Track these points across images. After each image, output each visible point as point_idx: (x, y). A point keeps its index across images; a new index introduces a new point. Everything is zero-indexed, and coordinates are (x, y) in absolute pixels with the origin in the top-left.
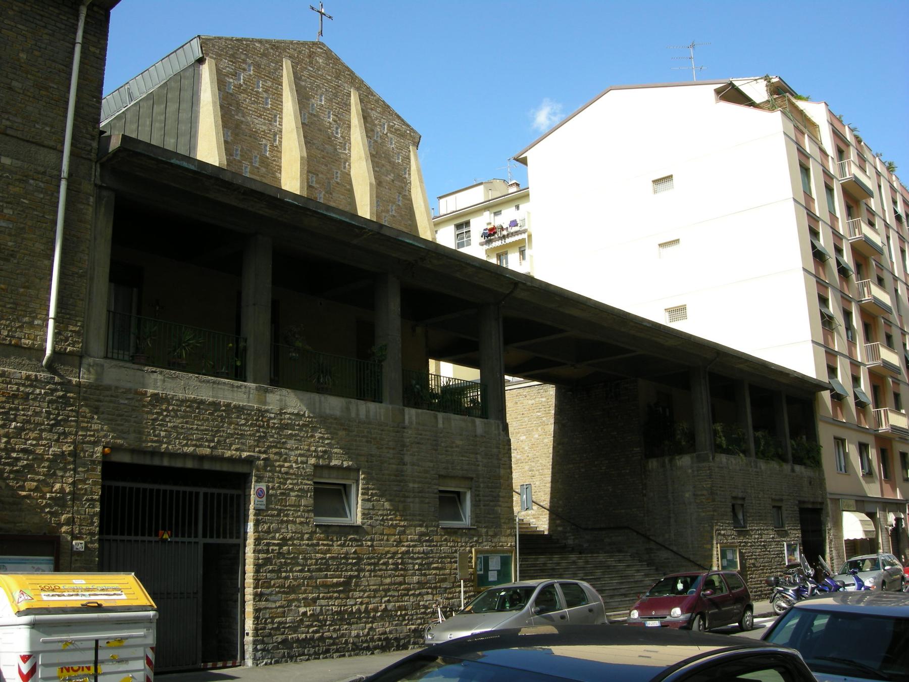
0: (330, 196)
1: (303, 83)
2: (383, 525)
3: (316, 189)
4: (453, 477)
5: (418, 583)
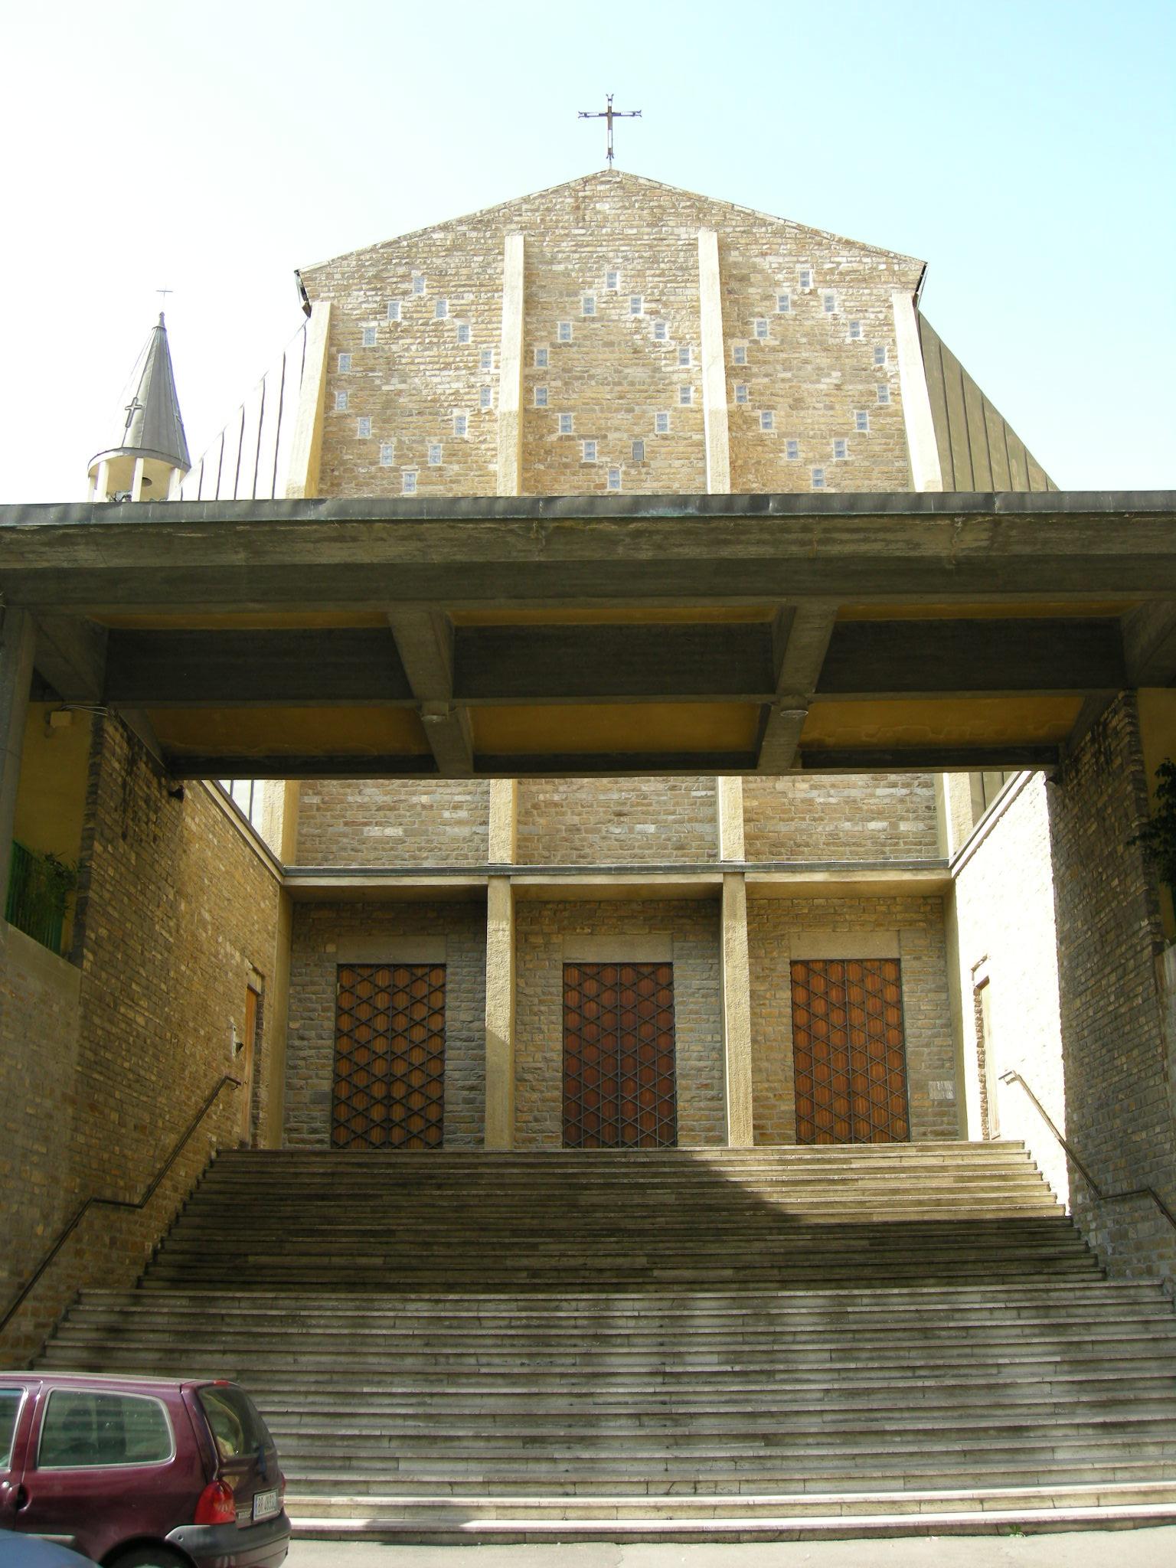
0: (644, 470)
1: (560, 268)
3: (601, 467)
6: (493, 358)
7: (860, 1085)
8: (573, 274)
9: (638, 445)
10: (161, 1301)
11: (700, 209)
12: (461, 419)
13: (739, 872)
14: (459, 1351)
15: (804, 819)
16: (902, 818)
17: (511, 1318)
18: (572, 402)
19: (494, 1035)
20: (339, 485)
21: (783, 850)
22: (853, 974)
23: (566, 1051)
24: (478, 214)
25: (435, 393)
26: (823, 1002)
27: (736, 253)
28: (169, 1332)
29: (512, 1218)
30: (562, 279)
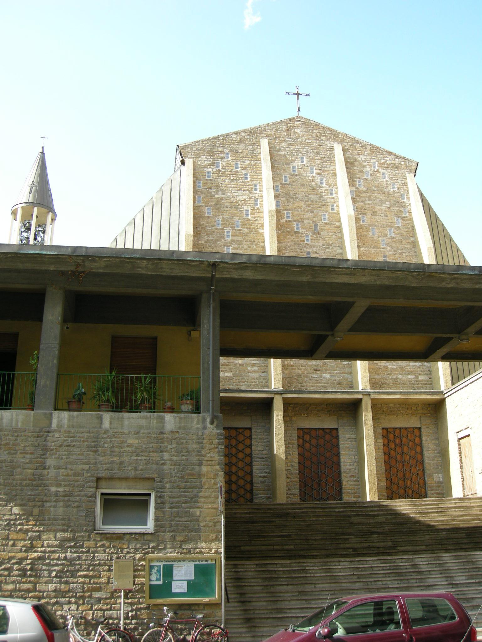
0: (319, 236)
1: (282, 153)
2: (9, 530)
3: (302, 233)
4: (126, 479)
5: (55, 591)
6: (258, 187)
7: (408, 475)
8: (288, 156)
9: (316, 226)
10: (245, 566)
11: (335, 135)
12: (247, 211)
13: (368, 394)
14: (375, 579)
15: (384, 374)
16: (420, 374)
17: (383, 566)
18: (290, 207)
19: (279, 457)
20: (200, 234)
21: (377, 385)
22: (404, 433)
23: (299, 463)
24: (249, 129)
25: (236, 200)
26: (393, 444)
27: (349, 153)
28: (260, 578)
29: (332, 529)
30: (283, 158)
